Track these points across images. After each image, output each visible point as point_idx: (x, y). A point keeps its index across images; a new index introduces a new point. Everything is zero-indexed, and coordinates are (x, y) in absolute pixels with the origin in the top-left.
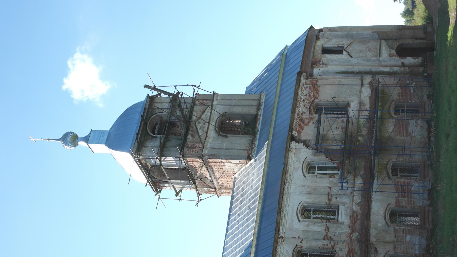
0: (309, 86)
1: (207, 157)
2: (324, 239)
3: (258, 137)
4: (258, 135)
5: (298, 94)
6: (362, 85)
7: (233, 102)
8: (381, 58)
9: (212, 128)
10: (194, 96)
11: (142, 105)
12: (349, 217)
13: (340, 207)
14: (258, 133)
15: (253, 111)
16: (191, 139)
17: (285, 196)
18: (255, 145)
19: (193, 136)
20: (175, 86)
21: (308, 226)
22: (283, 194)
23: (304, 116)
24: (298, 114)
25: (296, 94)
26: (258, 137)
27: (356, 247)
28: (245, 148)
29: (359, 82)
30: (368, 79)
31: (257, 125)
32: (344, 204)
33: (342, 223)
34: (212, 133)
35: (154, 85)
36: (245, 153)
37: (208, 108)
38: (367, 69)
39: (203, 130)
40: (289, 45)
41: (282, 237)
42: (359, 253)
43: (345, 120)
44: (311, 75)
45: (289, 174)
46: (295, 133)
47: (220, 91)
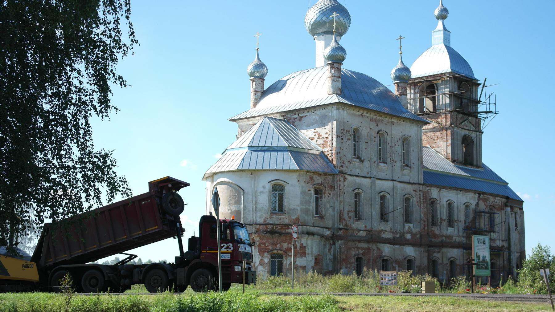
0: (501, 204)
1: (452, 130)
2: (441, 219)
3: (463, 167)
4: (472, 169)
5: (497, 197)
6: (503, 241)
7: (478, 147)
8: (516, 253)
9: (467, 132)
10: (479, 117)
11: (473, 76)
12: (450, 234)
13: (453, 228)
14: (465, 167)
15: (475, 163)
16: (460, 117)
17: (455, 191)
18: (460, 165)
19: (461, 118)
20: (495, 104)
21: (445, 208)
22: (457, 190)
23: (488, 202)
24: (489, 198)
25: (497, 196)
26: (463, 167)
27: (439, 240)
28: (458, 158)
29: (503, 239)
30: (506, 244)
31: (469, 166)
32: (454, 231)
33: (447, 230)
34: (464, 132)
35: (486, 86)
36: (456, 159)
37: (475, 129)
38: (512, 244)
39: (464, 125)
40: (508, 185)
41: (440, 190)
42: (438, 241)
43: (488, 230)
44: (506, 205)
45: (465, 193)
46: (482, 196)
47: (484, 136)
